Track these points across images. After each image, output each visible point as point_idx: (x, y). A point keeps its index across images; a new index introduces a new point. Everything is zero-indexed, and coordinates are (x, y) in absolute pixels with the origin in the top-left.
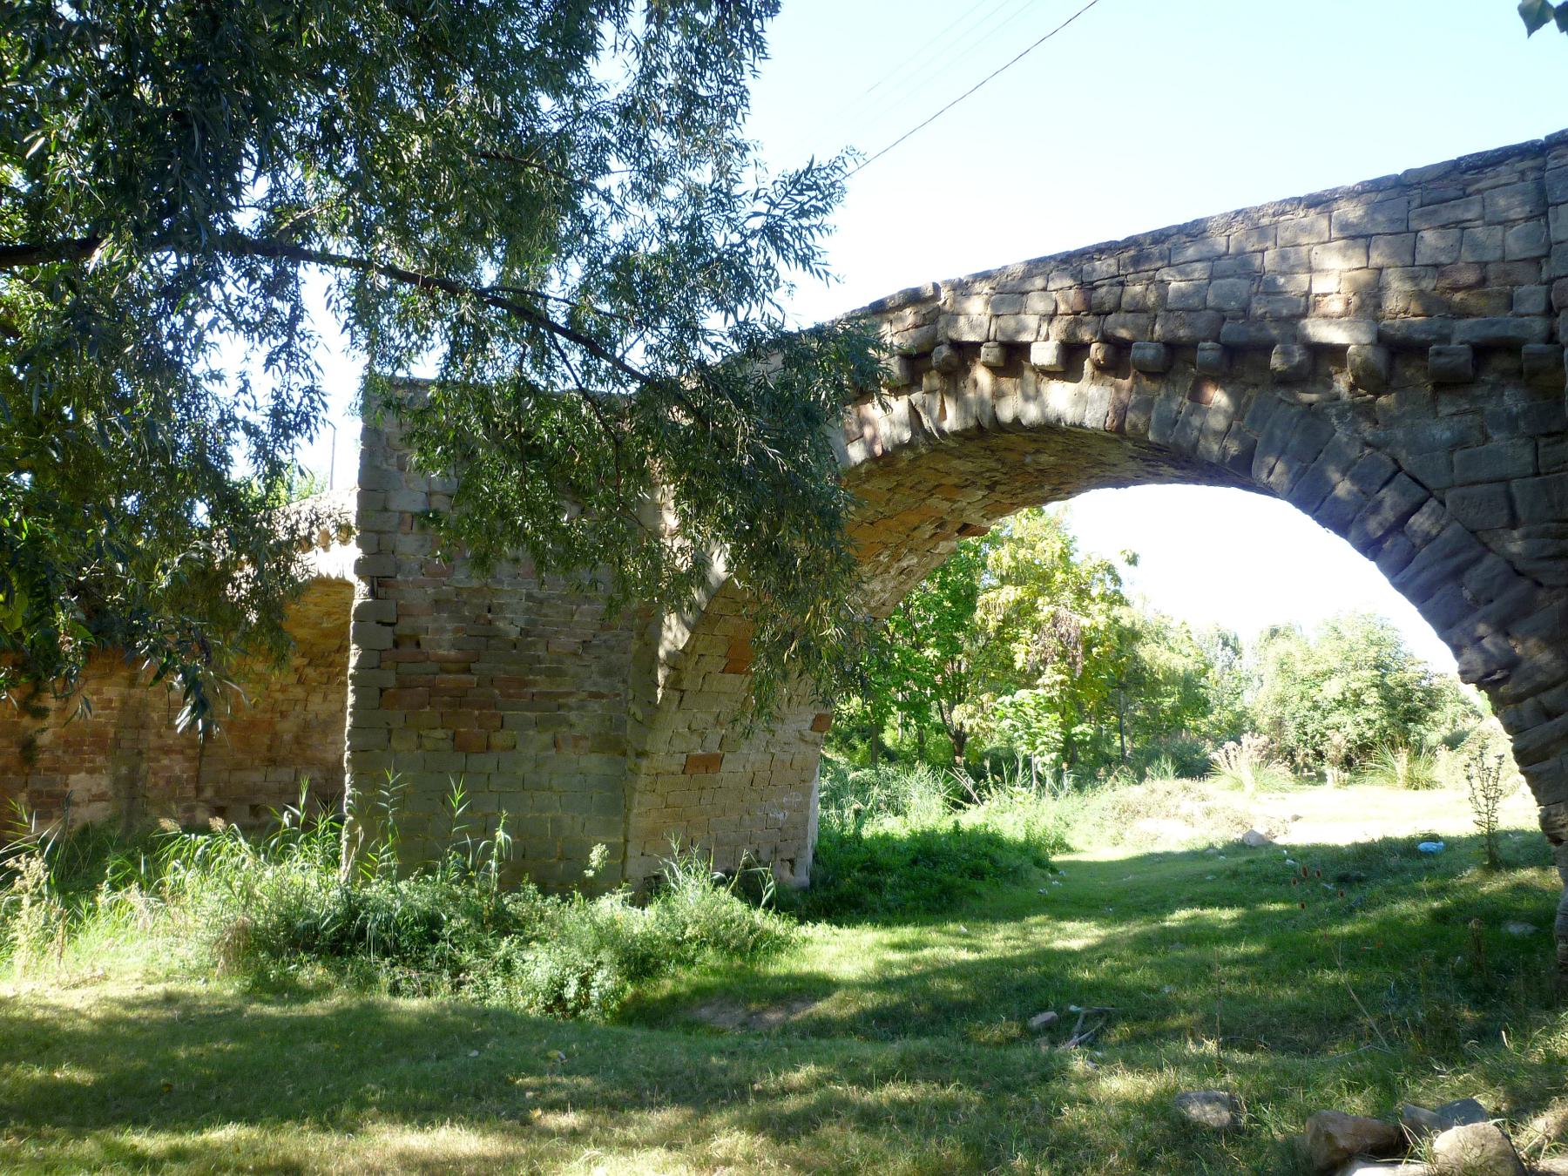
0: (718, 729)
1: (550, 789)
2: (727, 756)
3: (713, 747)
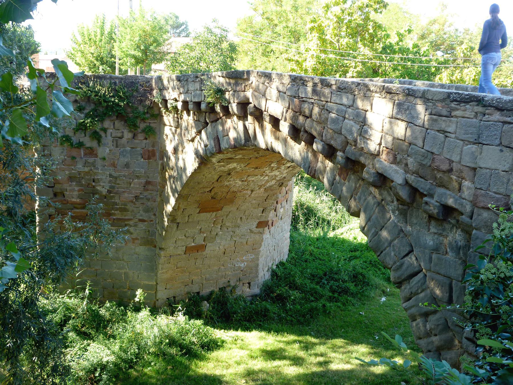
0: (202, 234)
1: (123, 260)
2: (209, 244)
3: (199, 240)
